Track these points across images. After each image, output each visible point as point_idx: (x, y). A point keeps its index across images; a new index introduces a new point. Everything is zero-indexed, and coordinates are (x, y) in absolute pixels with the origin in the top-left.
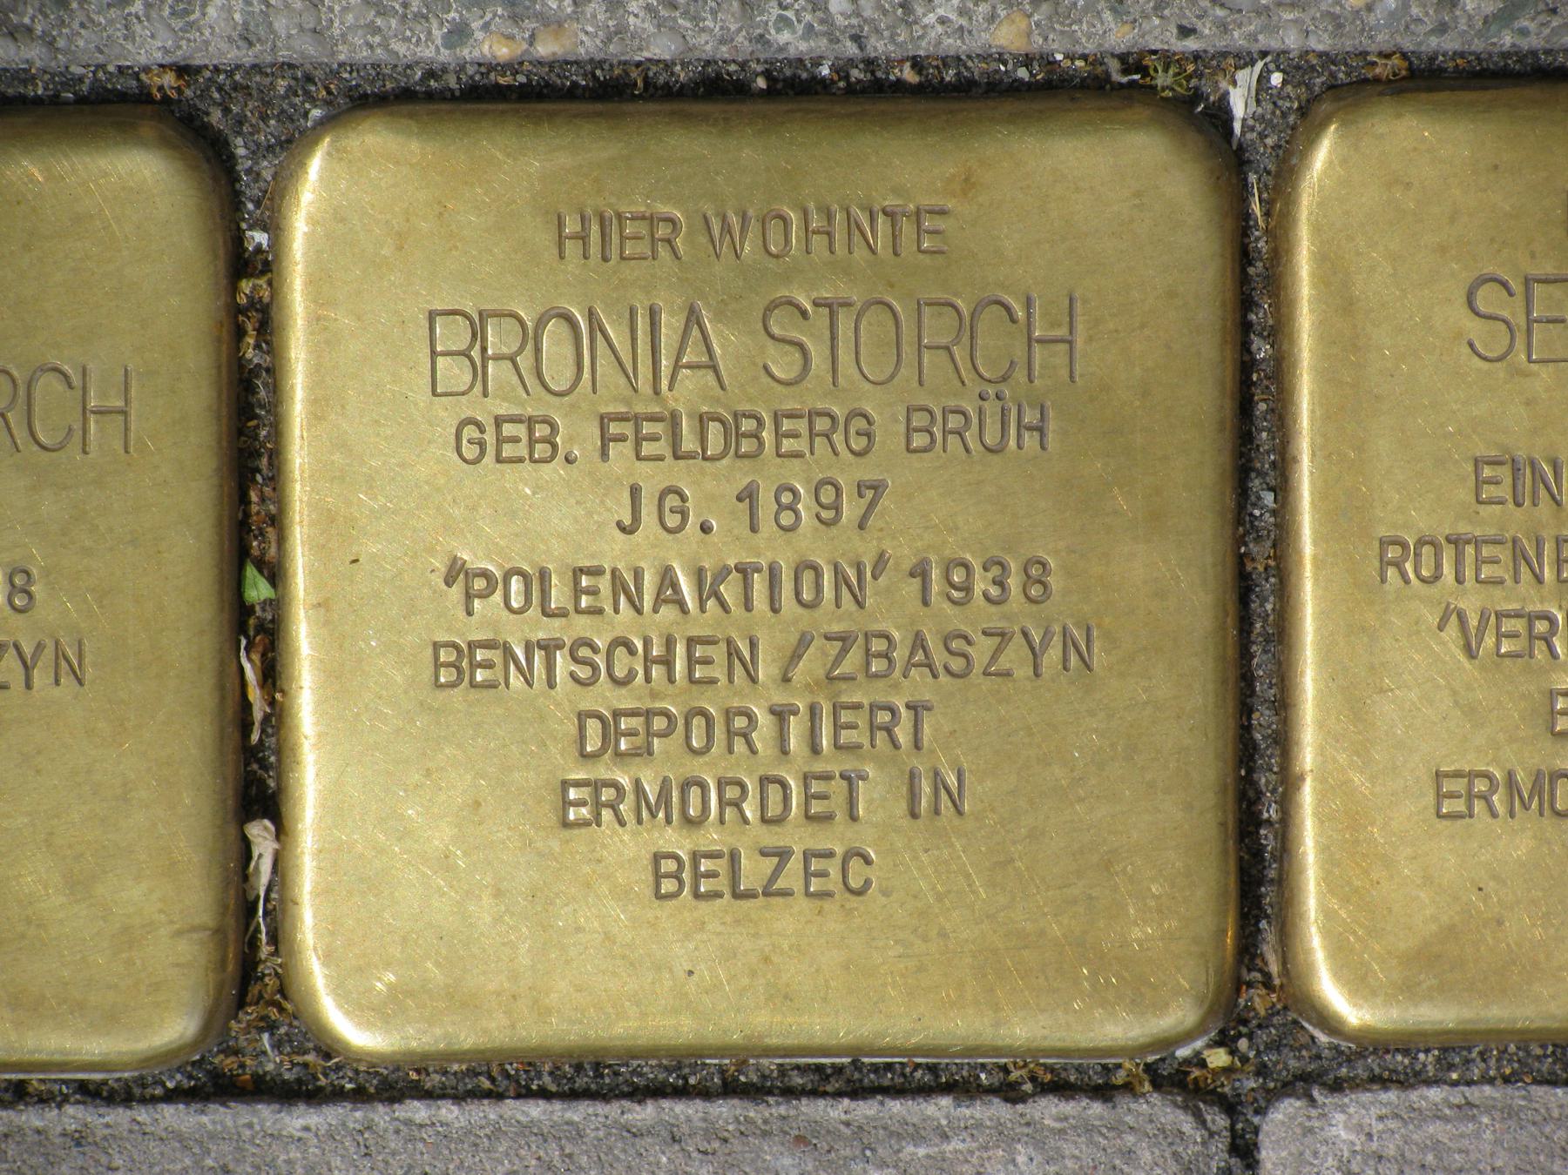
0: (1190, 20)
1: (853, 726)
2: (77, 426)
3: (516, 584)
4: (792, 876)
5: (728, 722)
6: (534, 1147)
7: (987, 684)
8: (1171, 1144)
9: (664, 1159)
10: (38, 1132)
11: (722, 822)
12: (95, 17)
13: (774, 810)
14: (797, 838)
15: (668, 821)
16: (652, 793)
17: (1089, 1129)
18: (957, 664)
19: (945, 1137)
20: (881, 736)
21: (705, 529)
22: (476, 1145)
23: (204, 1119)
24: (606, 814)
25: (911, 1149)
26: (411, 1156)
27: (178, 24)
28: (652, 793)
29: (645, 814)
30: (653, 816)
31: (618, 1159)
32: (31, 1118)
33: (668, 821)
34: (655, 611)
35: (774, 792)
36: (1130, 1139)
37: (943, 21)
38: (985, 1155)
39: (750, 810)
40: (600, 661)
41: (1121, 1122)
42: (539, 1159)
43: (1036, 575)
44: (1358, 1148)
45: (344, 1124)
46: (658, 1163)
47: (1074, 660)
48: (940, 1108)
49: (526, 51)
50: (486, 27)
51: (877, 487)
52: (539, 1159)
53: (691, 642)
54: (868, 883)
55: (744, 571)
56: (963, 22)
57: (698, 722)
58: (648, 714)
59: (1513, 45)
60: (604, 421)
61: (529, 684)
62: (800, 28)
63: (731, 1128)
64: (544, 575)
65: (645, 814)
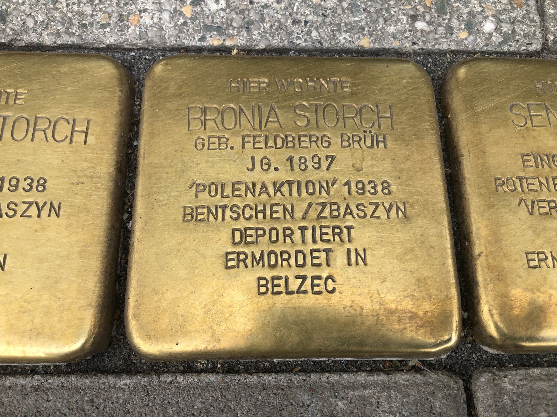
0: (415, 40)
1: (327, 234)
2: (69, 135)
3: (213, 187)
4: (307, 285)
5: (284, 232)
6: (211, 393)
7: (372, 220)
8: (447, 390)
9: (260, 397)
10: (22, 386)
11: (282, 266)
12: (95, 31)
13: (301, 262)
14: (309, 271)
15: (263, 266)
16: (258, 256)
17: (417, 385)
18: (362, 214)
19: (365, 388)
20: (337, 238)
21: (276, 169)
22: (190, 391)
23: (87, 381)
24: (241, 264)
25: (352, 392)
26: (164, 396)
27: (119, 33)
28: (258, 256)
29: (255, 263)
30: (258, 264)
31: (243, 397)
32: (9, 381)
33: (263, 266)
34: (259, 195)
35: (300, 256)
36: (432, 388)
37: (345, 38)
38: (380, 395)
39: (292, 261)
40: (241, 211)
41: (427, 381)
42: (213, 397)
43: (386, 186)
44: (515, 391)
45: (140, 383)
46: (258, 398)
47: (401, 214)
48: (362, 377)
49: (223, 43)
50: (211, 37)
51: (333, 158)
52: (213, 397)
53: (272, 206)
54: (334, 289)
55: (290, 183)
56: (351, 39)
57: (274, 232)
58: (257, 229)
59: (508, 49)
60: (243, 137)
61: (216, 220)
62: (303, 40)
63: (285, 384)
64: (223, 185)
65: (255, 263)
